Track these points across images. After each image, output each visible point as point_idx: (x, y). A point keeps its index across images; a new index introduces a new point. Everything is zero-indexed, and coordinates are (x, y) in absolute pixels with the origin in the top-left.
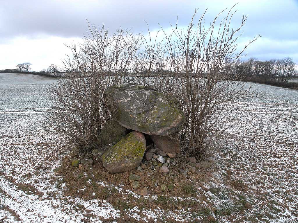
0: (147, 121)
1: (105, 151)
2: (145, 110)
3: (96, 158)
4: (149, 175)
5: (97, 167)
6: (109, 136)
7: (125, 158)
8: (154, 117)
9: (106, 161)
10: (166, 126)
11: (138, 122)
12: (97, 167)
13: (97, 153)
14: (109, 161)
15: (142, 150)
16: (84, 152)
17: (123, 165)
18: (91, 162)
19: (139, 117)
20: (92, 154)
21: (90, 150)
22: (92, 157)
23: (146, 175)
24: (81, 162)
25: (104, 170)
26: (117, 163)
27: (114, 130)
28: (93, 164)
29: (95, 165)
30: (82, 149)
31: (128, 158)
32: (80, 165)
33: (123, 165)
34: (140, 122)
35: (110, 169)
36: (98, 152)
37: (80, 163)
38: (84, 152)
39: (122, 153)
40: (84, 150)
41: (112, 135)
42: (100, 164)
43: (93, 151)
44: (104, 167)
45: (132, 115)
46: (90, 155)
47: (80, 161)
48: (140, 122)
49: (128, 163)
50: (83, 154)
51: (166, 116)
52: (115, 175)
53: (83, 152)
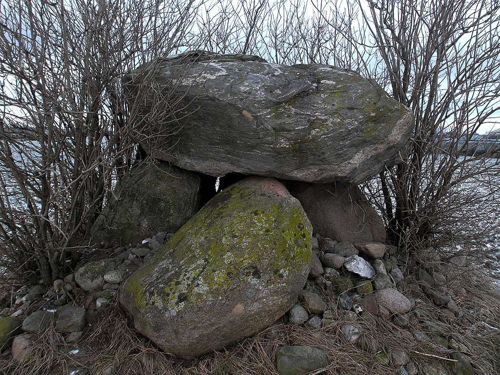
0: (312, 124)
1: (134, 265)
2: (294, 91)
3: (95, 300)
4: (354, 338)
5: (108, 341)
6: (142, 213)
7: (248, 274)
8: (334, 108)
9: (159, 304)
10: (375, 141)
11: (279, 130)
12: (106, 338)
13: (101, 277)
14: (176, 300)
15: (304, 236)
16: (41, 281)
17: (239, 308)
18: (76, 315)
19: (278, 116)
20: (78, 286)
21: (71, 262)
22: (77, 295)
23: (342, 339)
24: (24, 328)
25: (144, 350)
26: (214, 304)
27: (162, 187)
28: (86, 326)
29: (92, 330)
30: (33, 266)
31: (257, 274)
32: (20, 343)
33: (239, 308)
34: (284, 130)
35: (187, 339)
36: (103, 272)
37: (20, 332)
38: (41, 281)
39: (228, 257)
40: (38, 273)
41: (153, 206)
42: (120, 325)
43: (82, 270)
44: (140, 335)
45: (250, 111)
46: (68, 287)
47: (19, 320)
48: (284, 130)
49: (264, 297)
50: (34, 290)
51: (375, 103)
52: (208, 366)
53: (32, 281)
